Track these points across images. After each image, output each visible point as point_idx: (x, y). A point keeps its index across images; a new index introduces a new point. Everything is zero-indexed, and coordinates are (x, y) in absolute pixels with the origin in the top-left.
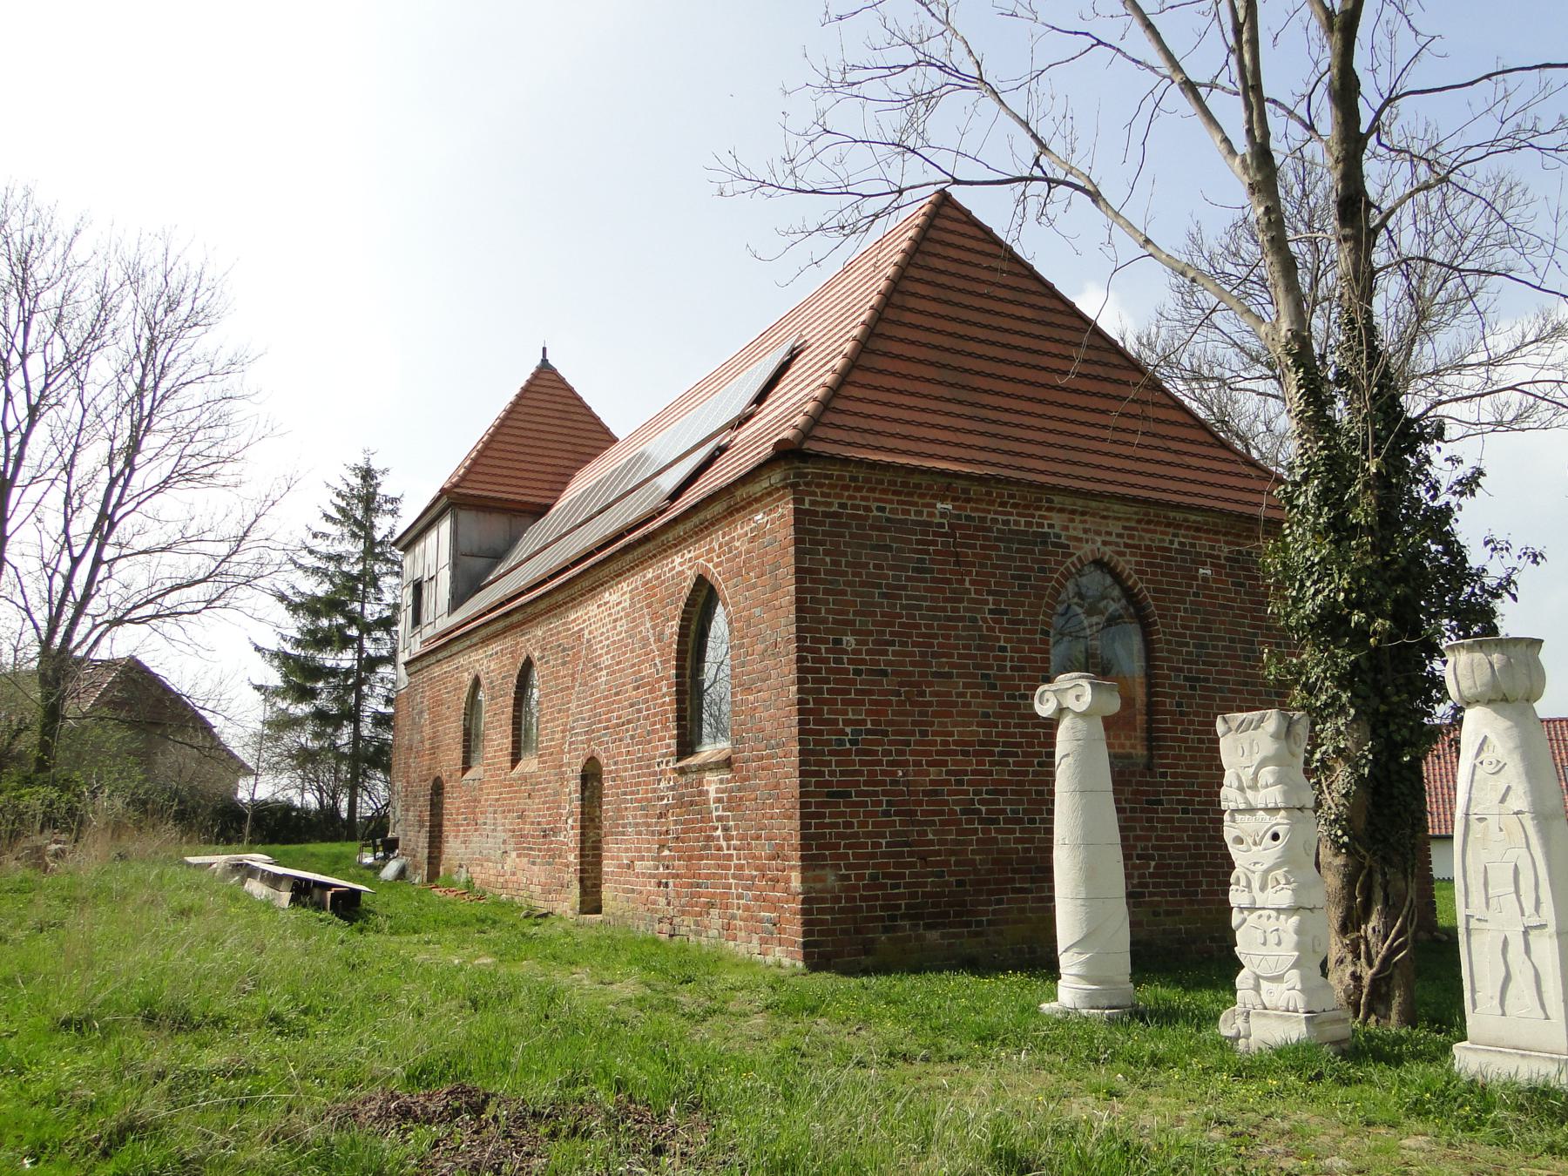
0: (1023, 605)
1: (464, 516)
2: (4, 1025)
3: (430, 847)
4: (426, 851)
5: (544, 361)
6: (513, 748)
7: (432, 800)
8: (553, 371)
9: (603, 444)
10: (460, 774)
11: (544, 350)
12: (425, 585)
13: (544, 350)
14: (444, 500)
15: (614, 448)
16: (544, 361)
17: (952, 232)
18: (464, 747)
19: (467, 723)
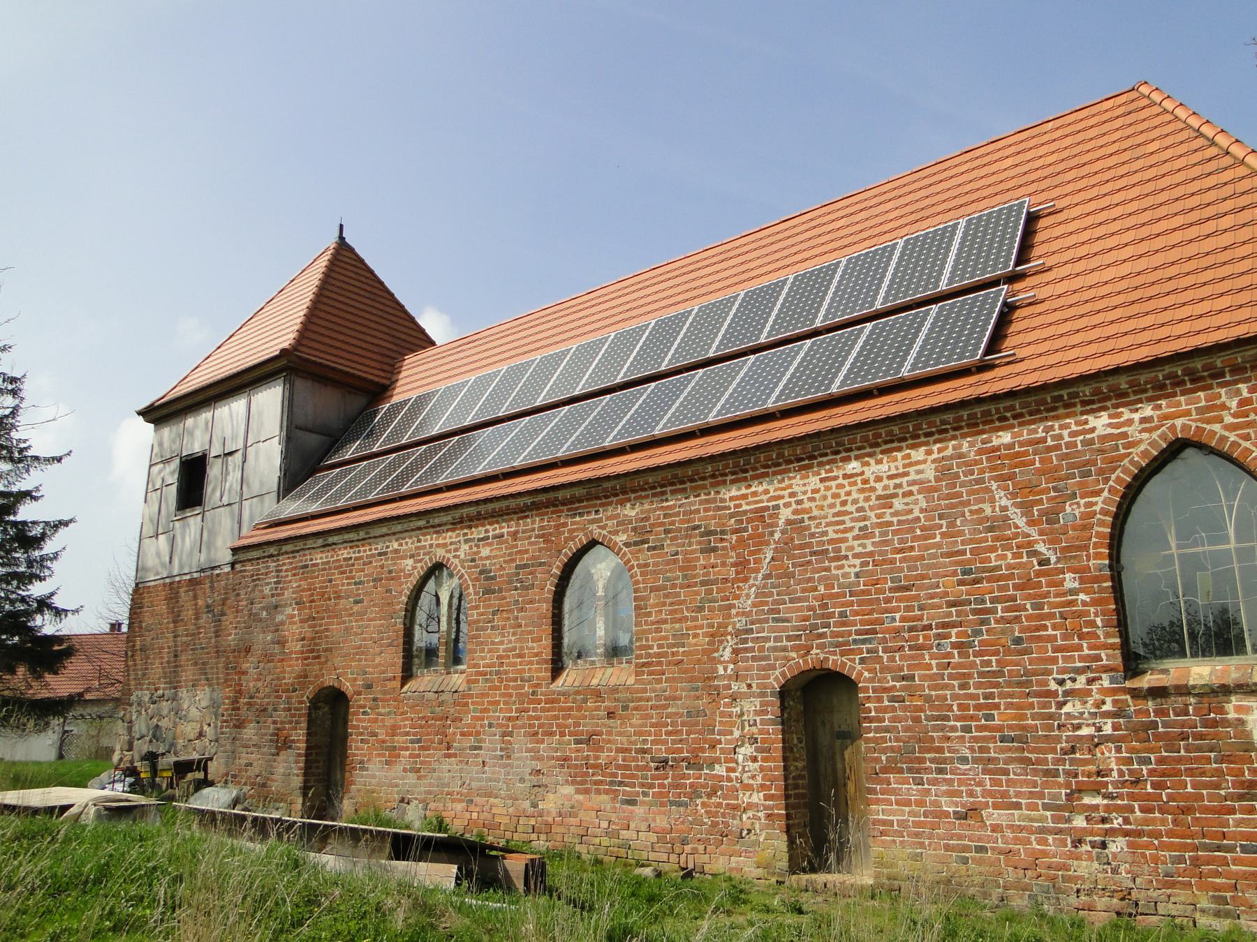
0: (1028, 618)
1: (300, 384)
2: (932, 938)
3: (305, 774)
4: (301, 779)
5: (341, 238)
6: (554, 654)
7: (309, 715)
8: (352, 250)
9: (413, 347)
10: (397, 683)
11: (341, 226)
12: (213, 471)
13: (341, 226)
14: (283, 362)
15: (430, 352)
16: (341, 238)
17: (317, 350)
18: (404, 650)
19: (407, 621)
